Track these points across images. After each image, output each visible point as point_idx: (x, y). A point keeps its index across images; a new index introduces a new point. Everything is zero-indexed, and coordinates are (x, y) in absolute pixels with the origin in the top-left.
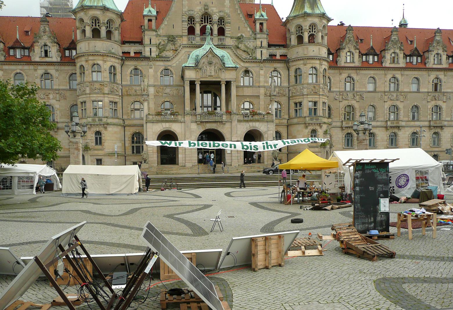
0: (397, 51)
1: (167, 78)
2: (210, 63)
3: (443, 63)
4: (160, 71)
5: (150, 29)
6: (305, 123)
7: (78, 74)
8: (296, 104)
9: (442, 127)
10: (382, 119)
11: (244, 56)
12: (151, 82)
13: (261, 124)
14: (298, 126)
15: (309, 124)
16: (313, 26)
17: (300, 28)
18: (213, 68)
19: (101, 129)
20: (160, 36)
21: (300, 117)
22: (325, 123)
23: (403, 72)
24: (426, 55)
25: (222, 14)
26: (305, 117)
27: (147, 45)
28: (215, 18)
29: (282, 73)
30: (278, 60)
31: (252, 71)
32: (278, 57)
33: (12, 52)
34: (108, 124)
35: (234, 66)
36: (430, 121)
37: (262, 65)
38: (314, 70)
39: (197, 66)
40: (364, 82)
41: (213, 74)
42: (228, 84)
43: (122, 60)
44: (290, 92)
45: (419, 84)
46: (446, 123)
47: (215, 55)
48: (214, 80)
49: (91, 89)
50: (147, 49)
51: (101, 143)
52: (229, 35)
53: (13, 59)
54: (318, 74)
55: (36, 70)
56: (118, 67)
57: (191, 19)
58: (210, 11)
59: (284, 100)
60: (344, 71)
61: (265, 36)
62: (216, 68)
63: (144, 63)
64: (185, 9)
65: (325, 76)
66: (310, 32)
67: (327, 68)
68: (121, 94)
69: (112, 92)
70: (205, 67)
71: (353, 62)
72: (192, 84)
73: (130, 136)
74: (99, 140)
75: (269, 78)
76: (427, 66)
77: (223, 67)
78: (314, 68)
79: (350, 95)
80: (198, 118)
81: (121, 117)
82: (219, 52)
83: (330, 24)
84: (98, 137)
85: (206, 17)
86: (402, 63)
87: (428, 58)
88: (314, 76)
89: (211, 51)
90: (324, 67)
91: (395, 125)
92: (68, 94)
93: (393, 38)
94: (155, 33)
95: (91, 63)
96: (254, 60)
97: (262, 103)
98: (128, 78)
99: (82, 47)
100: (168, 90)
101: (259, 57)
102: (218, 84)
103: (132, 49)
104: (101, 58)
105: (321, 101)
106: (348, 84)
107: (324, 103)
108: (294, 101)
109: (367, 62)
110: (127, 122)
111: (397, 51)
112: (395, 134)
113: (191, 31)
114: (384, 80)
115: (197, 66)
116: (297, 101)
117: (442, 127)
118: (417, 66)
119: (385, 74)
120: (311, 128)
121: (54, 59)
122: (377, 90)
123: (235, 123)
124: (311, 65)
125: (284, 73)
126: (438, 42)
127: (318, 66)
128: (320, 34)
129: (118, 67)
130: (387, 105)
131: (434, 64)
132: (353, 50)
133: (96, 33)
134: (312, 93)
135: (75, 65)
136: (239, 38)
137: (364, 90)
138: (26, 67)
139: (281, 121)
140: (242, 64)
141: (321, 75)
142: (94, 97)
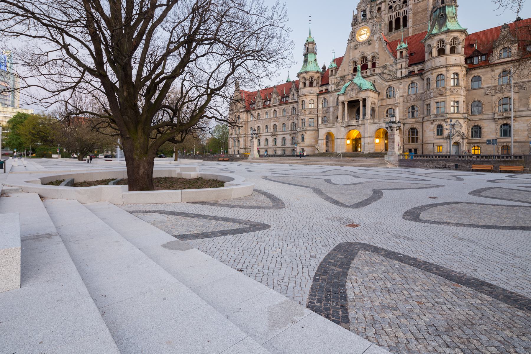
5: (332, 75)
11: (388, 77)
25: (373, 54)
28: (369, 58)
34: (306, 130)
37: (401, 81)
41: (354, 95)
42: (364, 100)
50: (330, 87)
54: (460, 78)
58: (365, 55)
60: (497, 67)
61: (404, 60)
63: (328, 95)
64: (351, 59)
72: (343, 103)
74: (303, 139)
77: (360, 89)
80: (345, 125)
84: (440, 129)
85: (364, 58)
96: (396, 79)
102: (358, 101)
103: (323, 89)
115: (345, 93)
120: (436, 123)
123: (367, 125)
124: (437, 74)
127: (459, 72)
129: (316, 100)
138: (286, 106)
139: (417, 120)
140: (387, 84)
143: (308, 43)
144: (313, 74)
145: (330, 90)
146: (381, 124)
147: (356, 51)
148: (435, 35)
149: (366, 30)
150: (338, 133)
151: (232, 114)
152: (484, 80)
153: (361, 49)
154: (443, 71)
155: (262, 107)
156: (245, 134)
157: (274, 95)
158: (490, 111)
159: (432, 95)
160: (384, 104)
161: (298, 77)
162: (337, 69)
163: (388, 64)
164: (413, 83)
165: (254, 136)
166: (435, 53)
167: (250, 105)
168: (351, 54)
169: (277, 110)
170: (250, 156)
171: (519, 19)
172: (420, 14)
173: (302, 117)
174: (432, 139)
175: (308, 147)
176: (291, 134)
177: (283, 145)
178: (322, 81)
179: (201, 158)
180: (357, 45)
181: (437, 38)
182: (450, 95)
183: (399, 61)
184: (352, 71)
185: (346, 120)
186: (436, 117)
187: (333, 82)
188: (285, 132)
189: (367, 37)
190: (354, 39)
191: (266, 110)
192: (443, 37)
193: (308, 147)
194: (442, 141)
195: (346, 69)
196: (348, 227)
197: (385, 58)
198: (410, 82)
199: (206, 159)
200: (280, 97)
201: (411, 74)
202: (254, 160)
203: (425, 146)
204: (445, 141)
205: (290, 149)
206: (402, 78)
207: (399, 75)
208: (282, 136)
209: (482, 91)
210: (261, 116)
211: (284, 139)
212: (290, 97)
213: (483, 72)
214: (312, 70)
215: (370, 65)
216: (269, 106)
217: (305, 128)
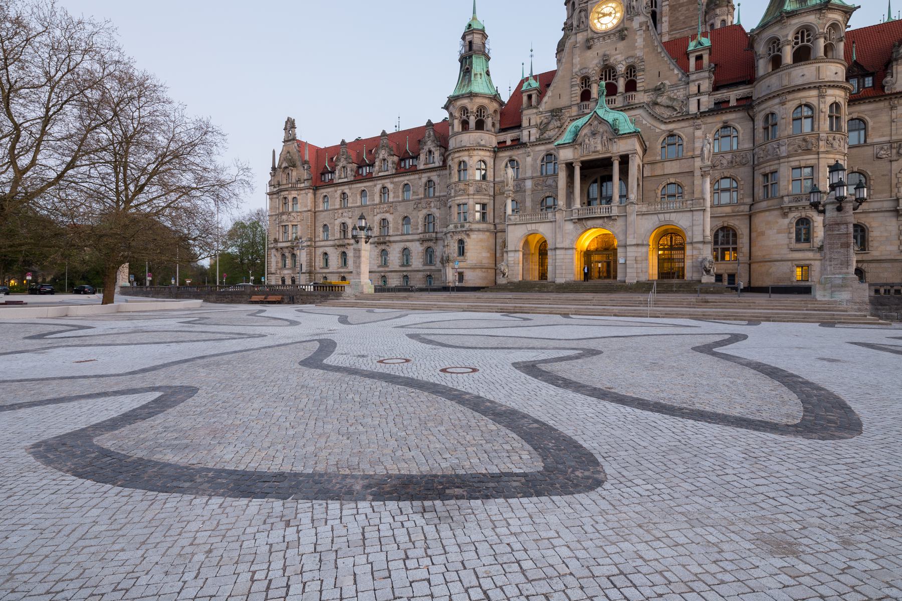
2: (594, 134)
4: (540, 158)
5: (530, 106)
6: (782, 208)
8: (766, 175)
11: (667, 113)
14: (767, 213)
15: (790, 208)
16: (805, 32)
20: (541, 113)
21: (772, 198)
25: (630, 60)
26: (782, 197)
27: (525, 128)
28: (621, 68)
30: (734, 107)
31: (682, 134)
32: (733, 103)
34: (471, 230)
38: (805, 109)
39: (574, 140)
41: (599, 148)
42: (624, 160)
43: (494, 152)
44: (756, 157)
47: (602, 121)
48: (601, 156)
49: (455, 191)
50: (525, 133)
52: (642, 89)
55: (420, 178)
59: (743, 173)
61: (706, 74)
62: (605, 138)
63: (521, 151)
64: (576, 70)
65: (837, 118)
66: (796, 43)
68: (492, 193)
69: (478, 191)
70: (587, 141)
72: (570, 166)
74: (462, 252)
77: (615, 133)
78: (806, 105)
80: (575, 216)
81: (492, 221)
83: (857, 22)
85: (608, 71)
90: (830, 100)
94: (535, 111)
95: (456, 160)
96: (687, 117)
102: (607, 163)
103: (508, 137)
104: (466, 153)
108: (762, 171)
113: (586, 96)
115: (574, 142)
116: (767, 170)
120: (794, 215)
121: (437, 165)
123: (632, 218)
127: (814, 101)
128: (821, 43)
129: (490, 162)
134: (800, 151)
138: (412, 177)
143: (470, 29)
144: (485, 102)
145: (525, 139)
146: (667, 216)
147: (590, 54)
148: (792, 14)
149: (614, 5)
150: (559, 236)
151: (278, 193)
152: (873, 128)
153: (600, 48)
154: (811, 96)
155: (352, 178)
156: (310, 240)
157: (383, 154)
158: (886, 195)
159: (783, 151)
160: (659, 172)
161: (446, 107)
162: (541, 93)
163: (667, 82)
164: (726, 126)
165: (363, 234)
167: (323, 174)
168: (577, 60)
169: (390, 186)
170: (348, 290)
172: (684, 8)
173: (460, 199)
175: (473, 268)
176: (423, 241)
177: (403, 265)
178: (501, 122)
179: (196, 296)
180: (592, 38)
181: (796, 23)
182: (827, 152)
183: (693, 77)
184: (578, 99)
185: (577, 204)
186: (797, 200)
187: (533, 122)
188: (410, 237)
189: (615, 22)
190: (582, 26)
191: (361, 186)
192: (811, 19)
193: (473, 268)
194: (810, 255)
195: (564, 94)
197: (658, 70)
198: (721, 125)
199: (213, 297)
200: (396, 159)
201: (721, 107)
202: (361, 300)
204: (818, 256)
205: (420, 275)
206: (703, 114)
207: (693, 108)
208: (402, 245)
209: (869, 151)
210: (350, 200)
211: (406, 252)
212: (422, 157)
213: (872, 111)
214: (482, 91)
215: (621, 84)
216: (370, 178)
217: (467, 225)
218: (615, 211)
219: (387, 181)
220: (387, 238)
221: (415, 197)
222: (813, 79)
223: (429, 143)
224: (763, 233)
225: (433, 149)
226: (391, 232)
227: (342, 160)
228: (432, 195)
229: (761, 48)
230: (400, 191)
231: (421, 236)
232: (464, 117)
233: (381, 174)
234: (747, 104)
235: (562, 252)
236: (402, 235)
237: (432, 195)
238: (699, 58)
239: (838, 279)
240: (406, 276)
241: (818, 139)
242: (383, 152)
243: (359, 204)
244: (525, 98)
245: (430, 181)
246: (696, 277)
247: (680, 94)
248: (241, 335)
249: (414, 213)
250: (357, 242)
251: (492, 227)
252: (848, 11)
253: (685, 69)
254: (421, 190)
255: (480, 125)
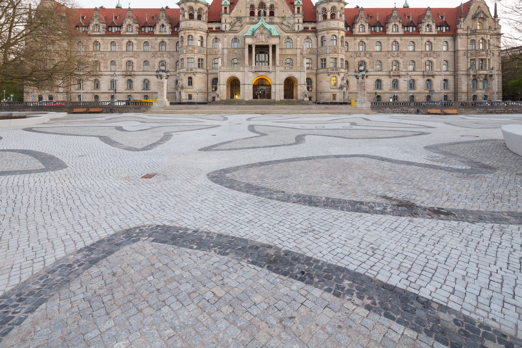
0: (397, 23)
1: (236, 44)
2: (262, 33)
3: (133, 31)
7: (180, 42)
8: (322, 59)
9: (433, 76)
10: (387, 70)
11: (287, 28)
12: (226, 46)
13: (296, 73)
16: (334, 8)
17: (324, 9)
18: (263, 36)
19: (192, 75)
20: (232, 17)
22: (342, 72)
23: (402, 38)
24: (420, 25)
25: (272, 2)
27: (223, 23)
28: (268, 5)
29: (312, 39)
32: (310, 29)
33: (110, 30)
34: (196, 72)
35: (278, 35)
36: (424, 72)
37: (298, 34)
39: (253, 35)
40: (373, 44)
41: (264, 40)
42: (274, 47)
43: (207, 32)
45: (414, 46)
46: (436, 73)
47: (265, 28)
49: (186, 50)
50: (223, 26)
51: (191, 85)
53: (143, 33)
56: (205, 37)
57: (252, 6)
59: (314, 57)
61: (301, 16)
63: (221, 34)
67: (344, 35)
69: (200, 52)
71: (364, 31)
72: (250, 47)
73: (211, 80)
74: (190, 83)
75: (303, 43)
76: (421, 33)
79: (362, 54)
80: (254, 70)
82: (268, 27)
83: (347, 7)
85: (262, 5)
86: (401, 31)
87: (421, 27)
88: (335, 41)
89: (262, 26)
90: (341, 35)
91: (396, 74)
92: (175, 54)
93: (394, 14)
94: (228, 16)
95: (187, 34)
96: (294, 31)
97: (298, 59)
98: (211, 44)
99: (182, 25)
100: (236, 51)
101: (296, 29)
102: (267, 47)
103: (214, 26)
104: (193, 31)
105: (340, 57)
106: (361, 47)
107: (342, 59)
109: (375, 31)
110: (210, 71)
111: (397, 23)
112: (397, 81)
113: (252, 14)
114: (387, 43)
115: (253, 35)
117: (433, 76)
118: (413, 33)
119: (388, 40)
121: (168, 33)
122: (382, 50)
123: (278, 72)
124: (332, 34)
125: (314, 39)
126: (429, 17)
127: (337, 34)
128: (339, 14)
129: (205, 37)
130: (390, 60)
131: (393, 31)
132: (364, 24)
133: (191, 17)
135: (178, 37)
136: (283, 18)
137: (372, 50)
138: (151, 38)
140: (285, 34)
141: (340, 40)
142: (189, 55)
144: (203, 6)
157: (128, 21)
160: (284, 53)
165: (164, 74)
166: (187, 16)
170: (155, 105)
171: (129, 8)
174: (329, 89)
177: (144, 89)
183: (296, 16)
185: (254, 65)
186: (333, 70)
194: (336, 90)
196: (144, 179)
201: (306, 30)
203: (318, 94)
212: (158, 27)
218: (271, 69)
219: (133, 38)
220: (133, 73)
221: (152, 50)
222: (337, 27)
223: (163, 20)
224: (321, 82)
225: (165, 24)
226: (135, 69)
227: (95, 20)
228: (164, 50)
229: (319, 10)
230: (142, 45)
231: (124, 73)
232: (191, 12)
233: (127, 33)
234: (315, 31)
235: (247, 86)
236: (144, 71)
237: (164, 50)
238: (298, 8)
239: (363, 100)
240: (147, 96)
241: (338, 48)
242: (129, 20)
243: (109, 50)
244: (223, 9)
245: (163, 42)
246: (302, 98)
247: (292, 21)
248: (201, 122)
249: (152, 59)
250: (161, 78)
251: (206, 71)
252: (346, 4)
253: (293, 11)
254: (157, 46)
255: (199, 17)
